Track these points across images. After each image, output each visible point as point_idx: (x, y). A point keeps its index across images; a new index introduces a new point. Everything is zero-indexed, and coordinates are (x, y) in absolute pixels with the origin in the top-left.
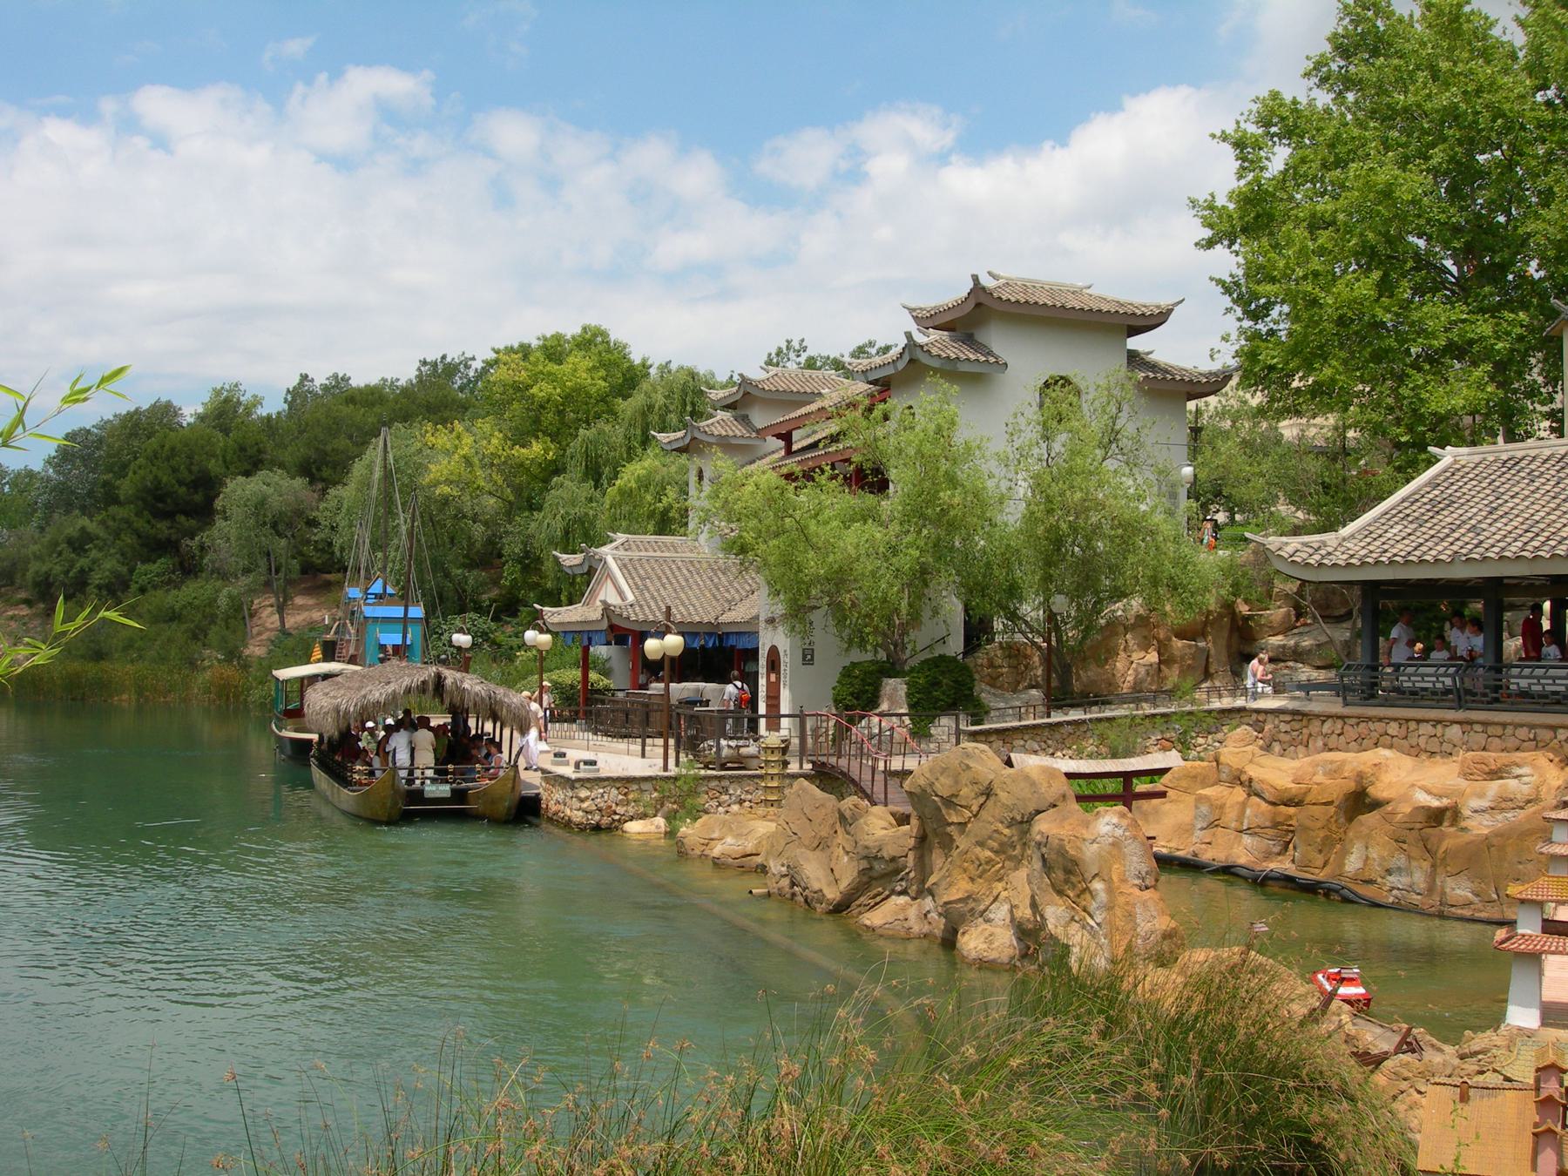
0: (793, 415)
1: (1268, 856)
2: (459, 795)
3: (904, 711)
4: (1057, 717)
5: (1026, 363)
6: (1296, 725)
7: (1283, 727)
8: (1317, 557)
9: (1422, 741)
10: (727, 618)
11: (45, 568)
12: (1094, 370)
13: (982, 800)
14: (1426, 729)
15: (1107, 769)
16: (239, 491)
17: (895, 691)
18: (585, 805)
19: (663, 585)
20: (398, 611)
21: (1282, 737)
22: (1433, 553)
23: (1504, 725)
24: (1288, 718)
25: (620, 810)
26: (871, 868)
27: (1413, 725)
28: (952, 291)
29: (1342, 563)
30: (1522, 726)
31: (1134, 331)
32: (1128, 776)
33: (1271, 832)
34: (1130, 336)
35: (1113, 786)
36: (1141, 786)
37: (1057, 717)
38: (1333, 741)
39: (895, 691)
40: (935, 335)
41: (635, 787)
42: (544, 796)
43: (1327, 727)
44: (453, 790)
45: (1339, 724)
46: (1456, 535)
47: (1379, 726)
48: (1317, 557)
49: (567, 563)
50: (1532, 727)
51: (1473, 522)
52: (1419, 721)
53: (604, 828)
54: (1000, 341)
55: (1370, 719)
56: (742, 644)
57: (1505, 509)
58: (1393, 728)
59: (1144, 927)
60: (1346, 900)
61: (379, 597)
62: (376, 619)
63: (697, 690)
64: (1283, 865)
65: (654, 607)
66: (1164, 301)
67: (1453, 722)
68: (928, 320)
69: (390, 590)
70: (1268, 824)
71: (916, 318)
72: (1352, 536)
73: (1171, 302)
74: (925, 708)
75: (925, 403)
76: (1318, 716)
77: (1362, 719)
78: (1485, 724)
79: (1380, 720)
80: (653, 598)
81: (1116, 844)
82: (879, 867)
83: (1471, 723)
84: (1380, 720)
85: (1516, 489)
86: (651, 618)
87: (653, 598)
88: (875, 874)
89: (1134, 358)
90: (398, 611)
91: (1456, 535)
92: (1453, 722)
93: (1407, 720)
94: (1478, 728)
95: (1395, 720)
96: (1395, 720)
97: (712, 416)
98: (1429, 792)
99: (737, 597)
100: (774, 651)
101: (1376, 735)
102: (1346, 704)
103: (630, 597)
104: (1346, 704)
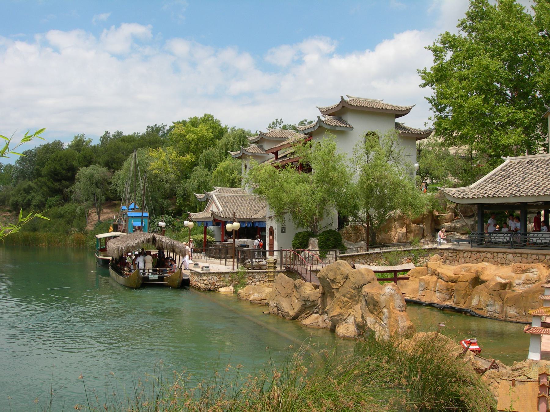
0: (278, 145)
1: (445, 300)
2: (161, 279)
3: (317, 249)
4: (371, 251)
5: (360, 127)
6: (455, 254)
7: (450, 255)
8: (462, 195)
9: (499, 260)
10: (255, 216)
11: (16, 199)
12: (384, 130)
13: (344, 280)
14: (500, 255)
15: (388, 270)
16: (84, 172)
17: (314, 242)
18: (205, 282)
19: (233, 205)
20: (139, 214)
21: (450, 258)
22: (503, 194)
23: (528, 254)
24: (452, 252)
25: (218, 284)
26: (306, 304)
27: (495, 254)
28: (334, 102)
29: (471, 197)
30: (534, 254)
31: (398, 116)
32: (396, 272)
33: (446, 291)
34: (396, 118)
35: (390, 276)
36: (400, 276)
37: (371, 251)
38: (467, 260)
39: (314, 242)
40: (328, 117)
41: (223, 276)
42: (191, 279)
43: (465, 255)
44: (159, 277)
45: (470, 254)
46: (511, 187)
47: (484, 254)
48: (462, 195)
49: (199, 197)
50: (537, 255)
51: (517, 183)
52: (498, 253)
53: (212, 290)
54: (351, 120)
55: (481, 252)
56: (260, 225)
57: (528, 178)
58: (489, 255)
59: (401, 325)
60: (472, 315)
61: (133, 209)
62: (132, 217)
63: (245, 242)
64: (450, 303)
65: (229, 212)
66: (408, 106)
67: (510, 253)
68: (325, 112)
69: (137, 207)
70: (445, 289)
71: (321, 111)
72: (474, 188)
73: (411, 106)
74: (324, 248)
75: (324, 141)
76: (462, 251)
77: (478, 252)
78: (521, 254)
79: (484, 252)
80: (229, 209)
81: (391, 296)
82: (308, 304)
83: (516, 253)
84: (484, 252)
85: (532, 171)
86: (228, 216)
87: (229, 209)
88: (307, 306)
89: (398, 125)
90: (139, 214)
91: (511, 187)
92: (510, 253)
93: (494, 252)
94: (518, 255)
95: (489, 252)
96: (489, 252)
97: (250, 146)
98: (501, 278)
99: (259, 209)
100: (271, 228)
101: (482, 257)
102: (472, 247)
103: (221, 209)
104: (472, 247)
